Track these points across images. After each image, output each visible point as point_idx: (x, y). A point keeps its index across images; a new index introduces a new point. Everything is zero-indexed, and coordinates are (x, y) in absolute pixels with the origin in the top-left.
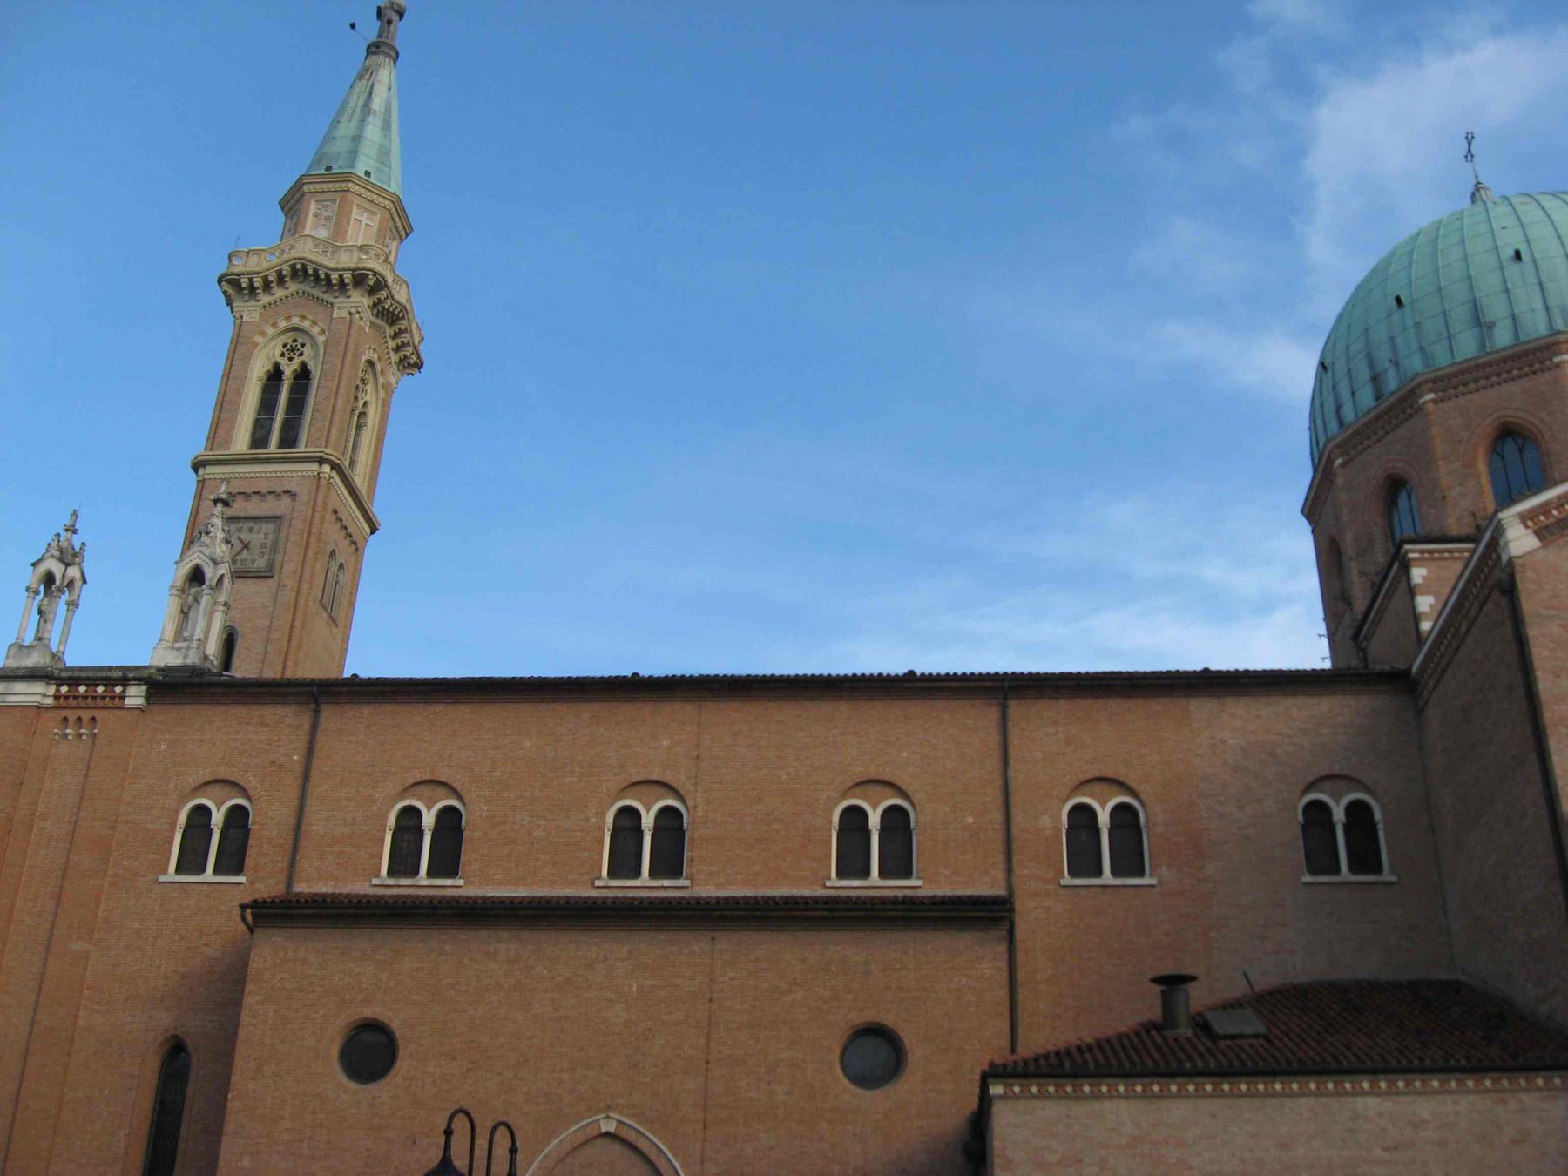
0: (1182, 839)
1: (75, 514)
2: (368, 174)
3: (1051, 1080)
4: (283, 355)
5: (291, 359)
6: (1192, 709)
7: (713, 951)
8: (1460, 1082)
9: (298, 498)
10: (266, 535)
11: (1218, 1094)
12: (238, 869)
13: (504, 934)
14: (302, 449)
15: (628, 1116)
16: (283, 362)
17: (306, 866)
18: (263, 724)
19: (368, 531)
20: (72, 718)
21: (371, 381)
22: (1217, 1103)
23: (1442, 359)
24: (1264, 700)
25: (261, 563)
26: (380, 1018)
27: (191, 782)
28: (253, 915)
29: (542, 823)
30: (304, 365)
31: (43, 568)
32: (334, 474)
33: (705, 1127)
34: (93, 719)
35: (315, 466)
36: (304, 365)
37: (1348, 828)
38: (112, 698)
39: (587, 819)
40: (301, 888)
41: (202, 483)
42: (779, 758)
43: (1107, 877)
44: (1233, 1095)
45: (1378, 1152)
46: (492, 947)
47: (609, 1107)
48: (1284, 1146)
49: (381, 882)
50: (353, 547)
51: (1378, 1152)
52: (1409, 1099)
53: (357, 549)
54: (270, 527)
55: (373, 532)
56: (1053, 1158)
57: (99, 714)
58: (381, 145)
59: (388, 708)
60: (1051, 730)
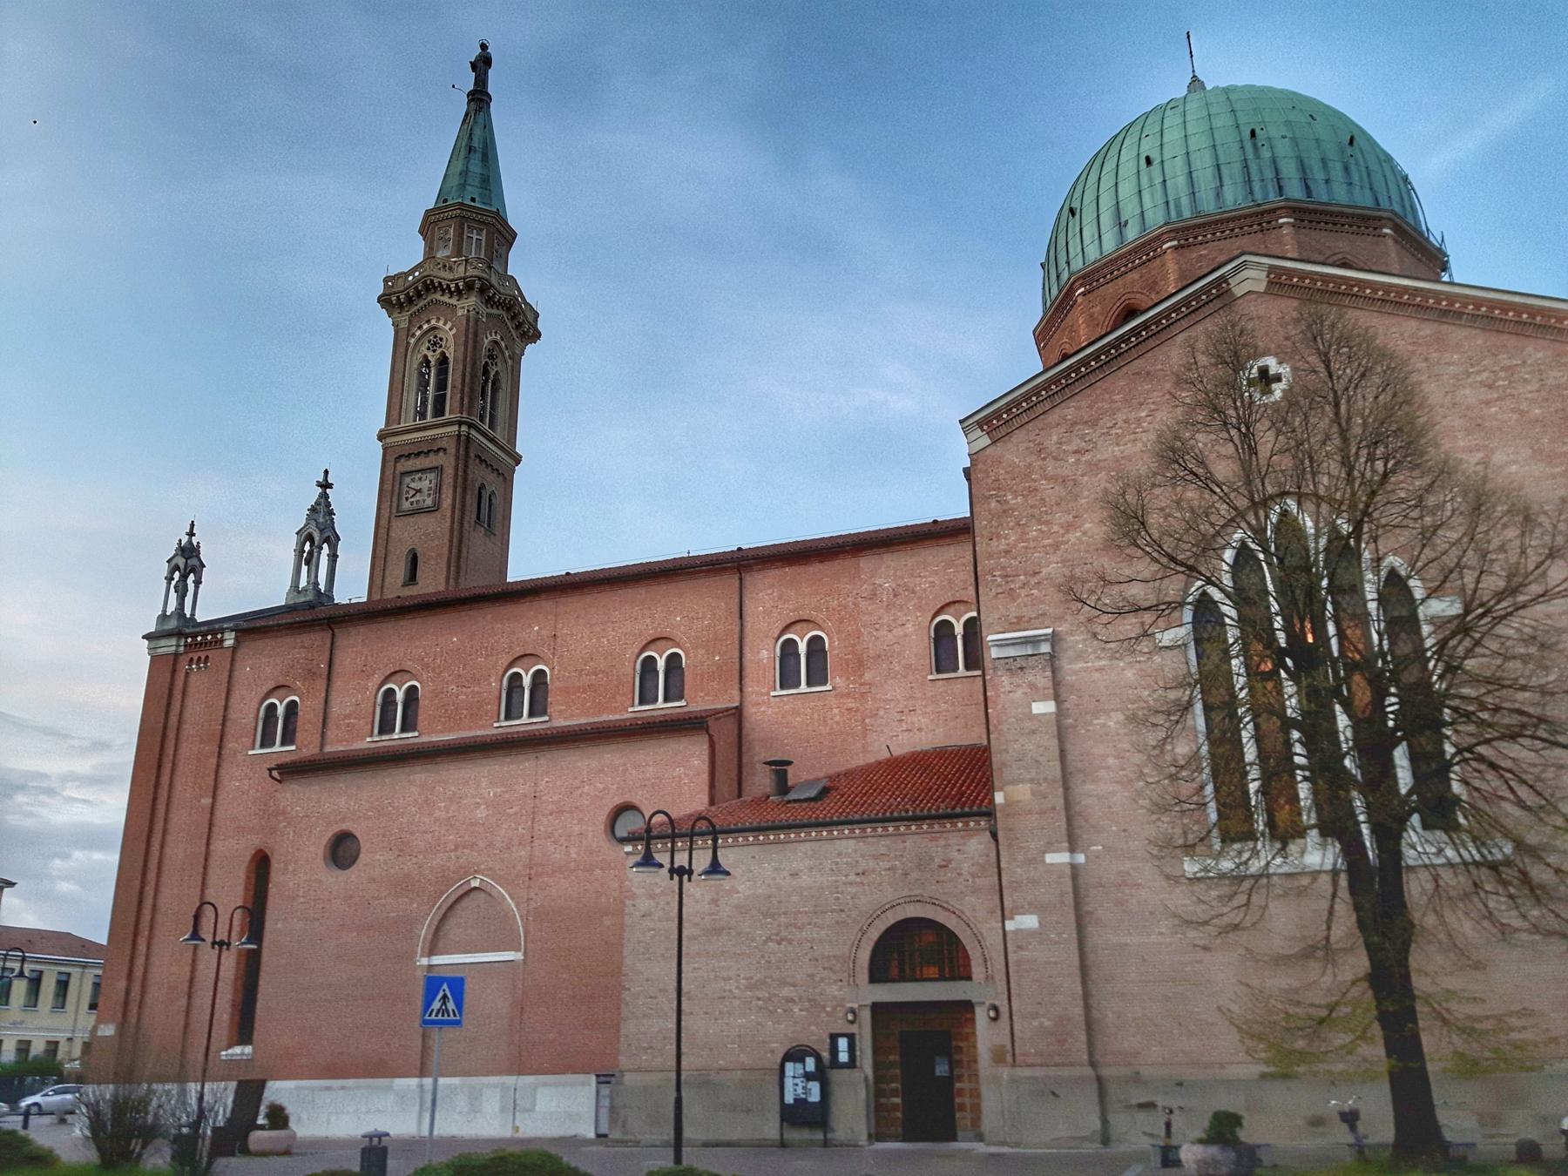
0: (850, 656)
1: (192, 524)
2: (473, 200)
3: (869, 825)
4: (429, 349)
5: (434, 351)
6: (861, 565)
7: (537, 765)
8: (908, 827)
9: (448, 452)
10: (431, 481)
11: (757, 843)
12: (292, 742)
13: (418, 768)
14: (447, 416)
15: (486, 876)
16: (430, 354)
17: (331, 734)
18: (303, 647)
19: (513, 463)
20: (195, 659)
21: (500, 356)
22: (756, 849)
23: (1208, 205)
24: (910, 553)
25: (429, 502)
26: (351, 829)
27: (265, 689)
28: (279, 773)
29: (464, 689)
30: (443, 354)
31: (174, 562)
32: (473, 432)
33: (530, 879)
34: (207, 657)
35: (456, 428)
36: (443, 354)
37: (965, 637)
38: (216, 642)
39: (490, 684)
40: (328, 749)
41: (385, 449)
42: (604, 630)
43: (803, 688)
44: (767, 843)
45: (852, 877)
46: (412, 777)
47: (476, 871)
48: (794, 875)
49: (371, 741)
50: (501, 478)
51: (852, 877)
52: (874, 840)
53: (505, 478)
54: (432, 476)
55: (518, 463)
56: (658, 891)
57: (210, 653)
58: (482, 174)
59: (374, 626)
60: (769, 591)
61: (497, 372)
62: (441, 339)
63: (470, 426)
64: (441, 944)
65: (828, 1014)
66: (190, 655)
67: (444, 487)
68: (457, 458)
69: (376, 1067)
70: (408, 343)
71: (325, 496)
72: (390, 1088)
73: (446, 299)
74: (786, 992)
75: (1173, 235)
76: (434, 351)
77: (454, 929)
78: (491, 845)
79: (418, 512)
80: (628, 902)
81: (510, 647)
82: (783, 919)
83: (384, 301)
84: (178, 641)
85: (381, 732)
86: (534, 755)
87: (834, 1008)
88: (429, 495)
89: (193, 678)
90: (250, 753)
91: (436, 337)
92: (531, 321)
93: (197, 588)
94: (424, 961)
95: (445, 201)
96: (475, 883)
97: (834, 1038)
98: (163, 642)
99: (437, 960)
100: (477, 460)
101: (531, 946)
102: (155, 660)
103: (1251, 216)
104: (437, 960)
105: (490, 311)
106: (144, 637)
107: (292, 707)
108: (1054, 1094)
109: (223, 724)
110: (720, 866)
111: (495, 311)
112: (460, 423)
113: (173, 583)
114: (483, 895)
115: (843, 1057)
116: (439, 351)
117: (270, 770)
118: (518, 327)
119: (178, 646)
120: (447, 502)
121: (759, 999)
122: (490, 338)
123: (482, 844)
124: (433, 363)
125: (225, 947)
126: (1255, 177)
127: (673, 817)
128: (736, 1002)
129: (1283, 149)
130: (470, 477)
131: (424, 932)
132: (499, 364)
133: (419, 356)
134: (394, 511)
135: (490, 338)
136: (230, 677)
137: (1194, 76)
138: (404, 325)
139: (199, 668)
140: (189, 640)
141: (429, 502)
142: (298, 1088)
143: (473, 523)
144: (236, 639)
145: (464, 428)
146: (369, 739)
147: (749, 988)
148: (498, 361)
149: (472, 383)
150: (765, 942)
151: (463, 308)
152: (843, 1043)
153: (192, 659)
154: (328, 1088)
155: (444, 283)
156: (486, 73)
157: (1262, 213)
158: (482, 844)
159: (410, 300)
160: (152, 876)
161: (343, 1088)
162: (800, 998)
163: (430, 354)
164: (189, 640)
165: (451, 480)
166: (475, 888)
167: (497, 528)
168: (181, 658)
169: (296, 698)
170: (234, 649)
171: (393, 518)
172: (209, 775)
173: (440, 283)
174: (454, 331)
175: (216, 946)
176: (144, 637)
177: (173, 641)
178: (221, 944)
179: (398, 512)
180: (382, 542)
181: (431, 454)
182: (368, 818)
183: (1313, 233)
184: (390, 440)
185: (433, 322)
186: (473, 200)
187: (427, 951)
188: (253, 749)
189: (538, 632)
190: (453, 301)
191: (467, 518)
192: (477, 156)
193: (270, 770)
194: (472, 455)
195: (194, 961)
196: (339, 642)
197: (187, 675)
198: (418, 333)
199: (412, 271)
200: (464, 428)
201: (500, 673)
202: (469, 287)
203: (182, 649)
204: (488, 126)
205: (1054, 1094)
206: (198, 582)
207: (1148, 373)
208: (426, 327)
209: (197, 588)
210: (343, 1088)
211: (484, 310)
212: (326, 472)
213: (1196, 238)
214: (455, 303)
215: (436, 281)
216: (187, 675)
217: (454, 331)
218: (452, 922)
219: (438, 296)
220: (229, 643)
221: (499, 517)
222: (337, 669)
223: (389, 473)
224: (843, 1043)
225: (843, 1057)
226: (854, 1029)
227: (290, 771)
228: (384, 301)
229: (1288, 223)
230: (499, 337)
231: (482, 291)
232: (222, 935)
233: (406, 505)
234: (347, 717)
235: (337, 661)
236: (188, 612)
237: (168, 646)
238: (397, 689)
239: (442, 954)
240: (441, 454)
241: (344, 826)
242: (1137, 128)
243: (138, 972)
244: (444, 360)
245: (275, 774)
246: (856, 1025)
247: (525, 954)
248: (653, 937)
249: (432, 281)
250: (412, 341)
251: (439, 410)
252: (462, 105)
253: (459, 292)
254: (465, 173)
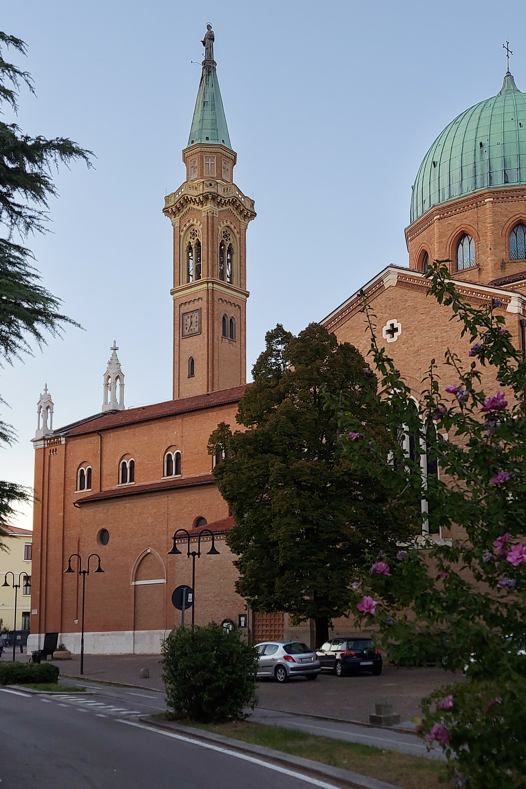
4: (191, 238)
5: (194, 239)
12: (90, 488)
16: (192, 241)
19: (245, 297)
34: (56, 449)
40: (104, 489)
54: (196, 314)
55: (248, 296)
57: (57, 447)
61: (230, 244)
62: (196, 231)
63: (213, 283)
64: (139, 575)
65: (239, 607)
66: (50, 448)
67: (203, 321)
68: (208, 303)
69: (119, 627)
70: (180, 236)
71: (115, 355)
72: (123, 634)
73: (195, 206)
74: (226, 598)
75: (438, 212)
76: (194, 239)
77: (143, 570)
78: (154, 534)
79: (191, 335)
80: (176, 563)
81: (166, 442)
82: (225, 570)
83: (166, 211)
84: (44, 442)
85: (123, 482)
86: (166, 496)
87: (240, 605)
88: (196, 325)
89: (52, 458)
90: (76, 492)
91: (194, 230)
92: (249, 208)
93: (51, 415)
94: (133, 583)
95: (193, 142)
96: (149, 551)
97: (240, 616)
98: (39, 443)
99: (138, 583)
100: (220, 301)
101: (169, 577)
102: (37, 450)
103: (473, 198)
104: (138, 583)
105: (221, 209)
106: (31, 441)
107: (90, 470)
108: (297, 637)
109: (65, 480)
110: (101, 569)
111: (225, 208)
112: (208, 283)
113: (41, 414)
114: (152, 556)
115: (243, 624)
116: (196, 238)
117: (74, 503)
118: (241, 212)
119: (44, 444)
120: (204, 329)
121: (217, 601)
122: (223, 226)
123: (150, 534)
124: (193, 247)
125: (87, 574)
126: (479, 173)
127: (187, 530)
128: (210, 602)
129: (497, 153)
130: (216, 313)
131: (132, 571)
132: (231, 239)
133: (187, 242)
134: (181, 336)
135: (223, 226)
136: (65, 458)
137: (508, 72)
138: (177, 225)
139: (54, 454)
140: (49, 441)
141: (197, 330)
142: (93, 635)
143: (220, 339)
144: (66, 440)
145: (210, 285)
146: (117, 486)
147: (215, 597)
148: (231, 237)
149: (213, 256)
150: (219, 579)
151: (205, 211)
152: (243, 619)
153: (50, 450)
154: (103, 635)
155: (193, 198)
156: (211, 46)
157: (478, 196)
158: (150, 534)
159: (178, 210)
160: (45, 547)
161: (108, 635)
162: (230, 601)
163: (192, 241)
164: (49, 441)
165: (206, 316)
166: (149, 553)
167: (237, 336)
168: (47, 450)
169: (90, 467)
170: (66, 444)
171: (181, 340)
172: (61, 503)
173: (191, 198)
174: (201, 226)
175: (82, 574)
176: (31, 441)
177: (42, 442)
178: (16, 586)
179: (183, 336)
180: (177, 354)
181: (192, 302)
182: (112, 523)
183: (503, 204)
184: (176, 295)
185: (191, 221)
186: (207, 139)
187: (134, 579)
188: (77, 490)
189: (176, 434)
190: (199, 208)
191: (216, 337)
192: (208, 108)
193: (74, 503)
194: (216, 299)
195: (62, 583)
196: (104, 441)
197: (50, 457)
198: (185, 229)
199: (178, 191)
200: (210, 285)
201: (163, 454)
202: (206, 198)
203: (46, 445)
204: (216, 85)
205: (297, 637)
206: (52, 413)
207: (352, 327)
208: (188, 225)
209: (51, 415)
210: (108, 635)
211: (217, 209)
212: (115, 342)
213: (447, 213)
214: (201, 209)
215: (189, 197)
216: (50, 457)
217: (201, 226)
218: (142, 567)
219: (192, 205)
220: (63, 442)
221: (237, 331)
222: (104, 453)
223: (177, 314)
224: (243, 619)
225: (243, 624)
226: (246, 612)
227: (83, 503)
228: (166, 211)
229: (490, 201)
230: (229, 223)
231: (214, 199)
232: (16, 583)
233: (186, 332)
234: (109, 475)
235: (104, 449)
236: (49, 427)
237: (41, 444)
238: (126, 462)
239: (140, 580)
240: (200, 301)
241: (103, 527)
242: (483, 104)
243: (44, 588)
244: (198, 244)
245: (77, 505)
246: (247, 611)
247: (167, 580)
248: (184, 577)
249: (187, 197)
250: (182, 234)
251: (198, 277)
252: (199, 70)
253: (201, 203)
254: (202, 120)
